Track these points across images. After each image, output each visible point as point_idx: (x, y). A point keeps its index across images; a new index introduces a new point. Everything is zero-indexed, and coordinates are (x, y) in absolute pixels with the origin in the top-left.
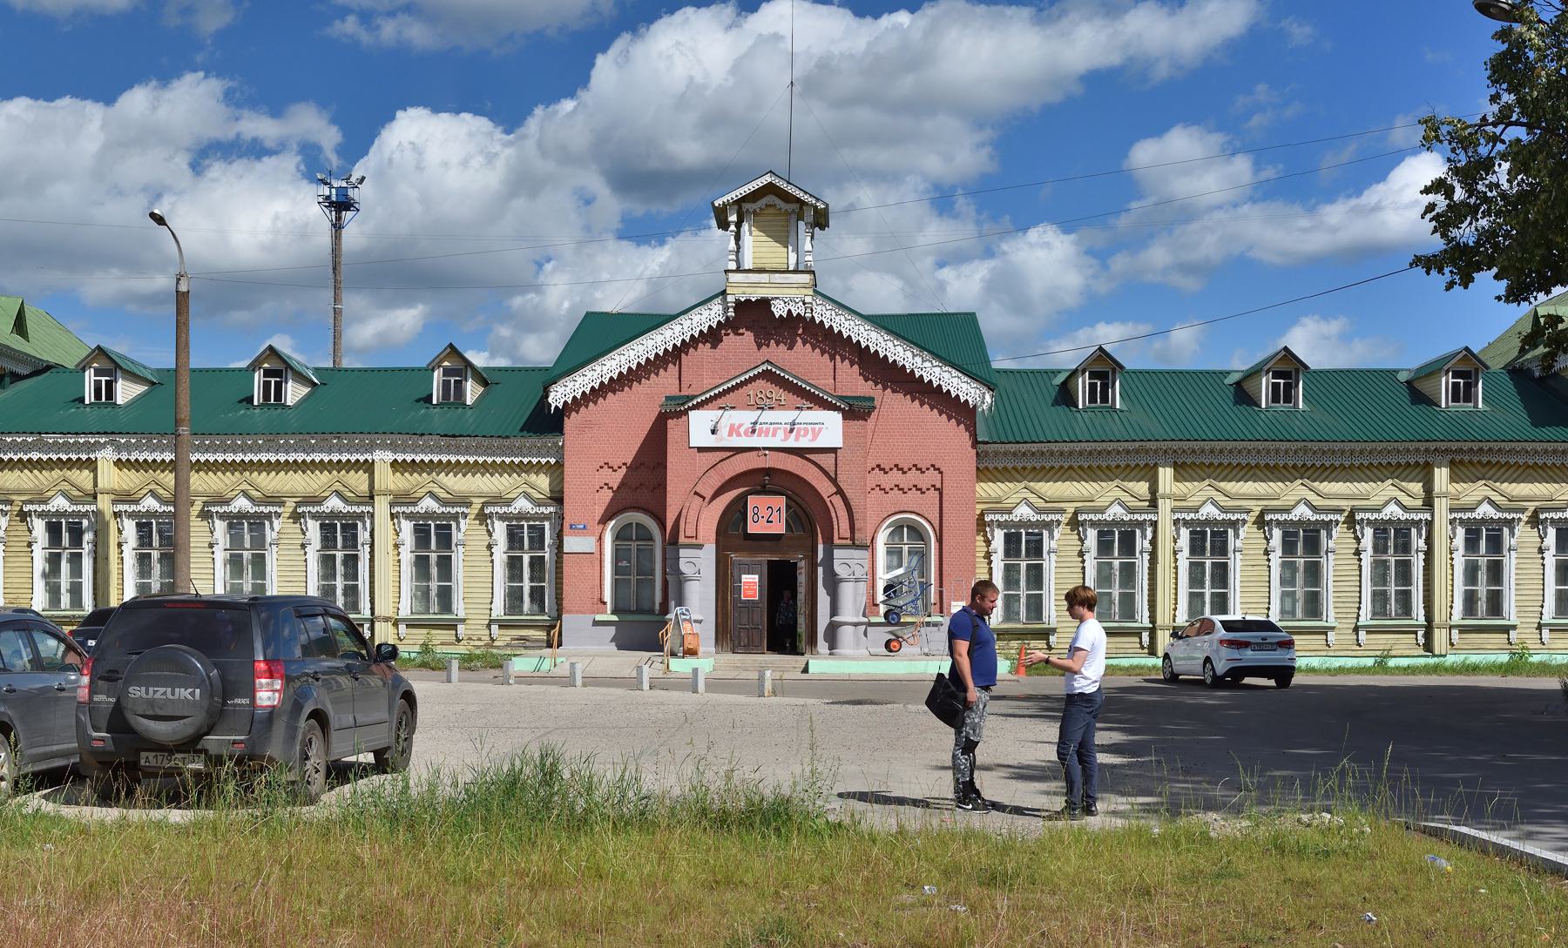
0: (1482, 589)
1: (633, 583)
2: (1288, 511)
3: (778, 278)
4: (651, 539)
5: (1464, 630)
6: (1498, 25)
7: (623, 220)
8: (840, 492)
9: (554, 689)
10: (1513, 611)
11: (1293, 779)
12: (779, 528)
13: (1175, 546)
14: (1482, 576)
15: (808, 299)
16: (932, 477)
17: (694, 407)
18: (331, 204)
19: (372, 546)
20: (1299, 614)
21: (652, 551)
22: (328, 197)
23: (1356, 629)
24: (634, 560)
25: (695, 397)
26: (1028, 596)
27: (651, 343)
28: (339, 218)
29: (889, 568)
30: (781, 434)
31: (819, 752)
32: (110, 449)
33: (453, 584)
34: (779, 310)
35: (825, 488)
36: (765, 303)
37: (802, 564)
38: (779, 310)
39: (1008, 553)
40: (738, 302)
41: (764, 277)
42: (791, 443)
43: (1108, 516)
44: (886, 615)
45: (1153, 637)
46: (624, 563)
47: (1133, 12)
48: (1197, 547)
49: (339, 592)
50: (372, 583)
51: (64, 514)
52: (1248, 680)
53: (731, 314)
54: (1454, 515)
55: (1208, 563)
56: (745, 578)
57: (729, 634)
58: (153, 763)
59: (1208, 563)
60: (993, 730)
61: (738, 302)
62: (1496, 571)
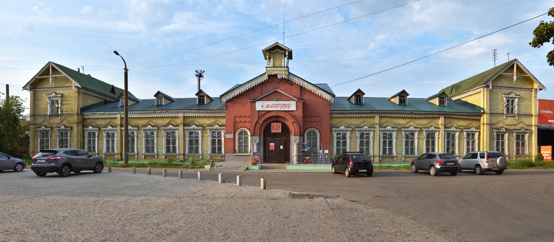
2: (362, 127)
3: (279, 69)
4: (247, 134)
12: (280, 131)
14: (451, 145)
19: (374, 138)
21: (316, 138)
30: (280, 107)
36: (276, 75)
38: (279, 77)
41: (275, 69)
42: (283, 109)
51: (171, 129)
56: (271, 144)
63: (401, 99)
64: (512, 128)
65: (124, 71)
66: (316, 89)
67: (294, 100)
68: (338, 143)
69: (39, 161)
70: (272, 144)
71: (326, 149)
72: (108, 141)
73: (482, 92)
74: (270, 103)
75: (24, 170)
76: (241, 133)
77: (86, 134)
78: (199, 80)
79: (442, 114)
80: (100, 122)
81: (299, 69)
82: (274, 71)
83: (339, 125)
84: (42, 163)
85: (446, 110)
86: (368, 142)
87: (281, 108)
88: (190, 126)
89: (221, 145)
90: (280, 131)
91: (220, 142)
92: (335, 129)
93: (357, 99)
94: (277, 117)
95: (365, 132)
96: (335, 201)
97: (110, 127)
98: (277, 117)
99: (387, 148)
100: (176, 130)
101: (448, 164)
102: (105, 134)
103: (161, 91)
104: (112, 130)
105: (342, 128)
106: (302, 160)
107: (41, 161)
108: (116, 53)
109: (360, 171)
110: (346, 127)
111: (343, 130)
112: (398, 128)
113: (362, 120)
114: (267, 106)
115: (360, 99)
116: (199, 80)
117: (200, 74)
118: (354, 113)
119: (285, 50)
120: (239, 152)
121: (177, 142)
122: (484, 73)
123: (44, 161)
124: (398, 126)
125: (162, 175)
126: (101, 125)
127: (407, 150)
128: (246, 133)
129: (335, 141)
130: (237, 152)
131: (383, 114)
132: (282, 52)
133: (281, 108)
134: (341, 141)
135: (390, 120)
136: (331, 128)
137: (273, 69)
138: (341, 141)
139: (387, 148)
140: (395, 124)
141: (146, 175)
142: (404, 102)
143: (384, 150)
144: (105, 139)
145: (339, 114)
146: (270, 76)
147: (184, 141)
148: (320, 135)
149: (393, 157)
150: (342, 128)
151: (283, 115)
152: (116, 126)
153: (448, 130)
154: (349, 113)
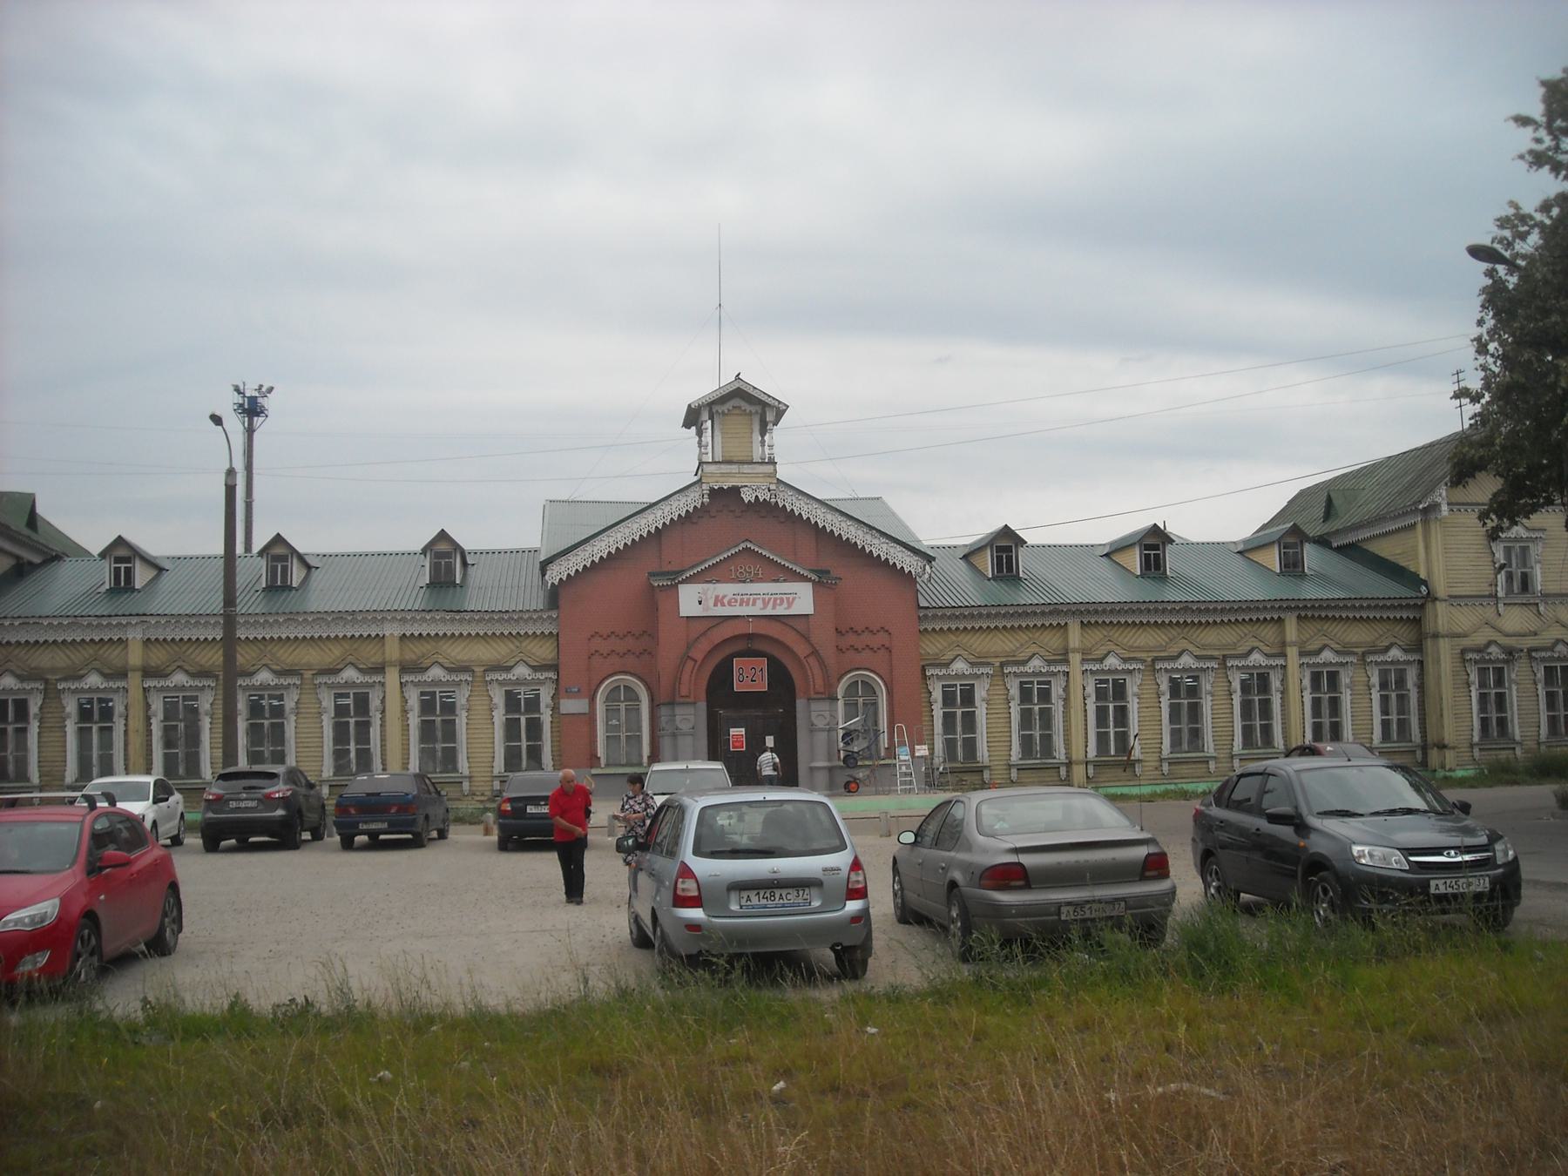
0: (1326, 721)
1: (623, 738)
2: (1024, 663)
3: (746, 469)
4: (637, 699)
5: (1097, 765)
6: (1485, 266)
7: (232, 1006)
8: (815, 653)
9: (1543, 878)
10: (1212, 745)
11: (607, 765)
12: (763, 686)
13: (1083, 687)
14: (1325, 710)
15: (773, 487)
16: (882, 638)
17: (683, 582)
18: (244, 411)
19: (383, 712)
20: (1185, 746)
21: (638, 710)
22: (241, 405)
23: (1232, 757)
24: (623, 718)
25: (684, 571)
26: (357, 723)
27: (636, 526)
28: (251, 423)
29: (847, 718)
30: (759, 603)
31: (310, 748)
32: (139, 629)
33: (1509, 715)
34: (747, 496)
35: (801, 650)
36: (735, 491)
37: (205, 703)
38: (747, 496)
39: (1022, 701)
40: (712, 490)
41: (734, 468)
42: (769, 611)
43: (1029, 668)
44: (845, 761)
45: (1425, 754)
46: (614, 722)
47: (505, 524)
48: (1101, 694)
49: (353, 755)
50: (383, 746)
51: (354, 685)
52: (382, 837)
53: (706, 500)
54: (1305, 660)
55: (1111, 706)
56: (733, 731)
57: (681, 810)
58: (1442, 890)
59: (1111, 706)
60: (353, 719)
61: (712, 490)
62: (1335, 704)
63: (1147, 557)
64: (1530, 642)
65: (1160, 803)
66: (868, 537)
67: (804, 579)
68: (949, 719)
69: (233, 804)
70: (738, 732)
71: (920, 743)
72: (84, 734)
73: (1419, 527)
74: (727, 589)
75: (1423, 576)
76: (613, 695)
77: (242, 706)
78: (250, 431)
79: (1289, 608)
80: (44, 659)
81: (809, 462)
82: (729, 475)
83: (949, 656)
84: (247, 809)
85: (1311, 592)
86: (1046, 716)
87: (765, 604)
88: (166, 676)
89: (1244, 727)
90: (763, 686)
91: (535, 728)
92: (936, 671)
93: (999, 559)
94: (749, 637)
95: (95, 696)
96: (1207, 1091)
97: (94, 680)
98: (750, 640)
99: (1112, 731)
100: (372, 685)
101: (531, 809)
102: (71, 707)
103: (130, 537)
104: (533, 682)
105: (960, 666)
106: (102, 775)
107: (243, 805)
108: (252, 409)
109: (545, 810)
110: (973, 664)
111: (964, 676)
112: (1143, 661)
113: (1023, 637)
114: (718, 601)
115: (1009, 559)
116: (250, 431)
117: (253, 400)
118: (997, 615)
119: (764, 405)
120: (607, 765)
121: (375, 732)
122: (1432, 445)
123: (254, 804)
124: (1143, 655)
125: (225, 765)
126: (53, 670)
127: (1248, 732)
128: (869, 688)
129: (938, 713)
130: (603, 762)
131: (1092, 615)
132: (753, 409)
133: (765, 604)
134: (959, 712)
135: (1115, 634)
136: (923, 669)
137: (725, 468)
138: (959, 712)
139: (1112, 731)
140: (1131, 649)
141: (387, 647)
142: (1157, 567)
143: (1102, 739)
144: (71, 728)
145: (1004, 616)
146: (715, 493)
147: (406, 728)
148: (890, 693)
149: (980, 771)
150: (960, 666)
151: (774, 630)
152: (122, 674)
153: (1313, 660)
154: (1164, 610)
